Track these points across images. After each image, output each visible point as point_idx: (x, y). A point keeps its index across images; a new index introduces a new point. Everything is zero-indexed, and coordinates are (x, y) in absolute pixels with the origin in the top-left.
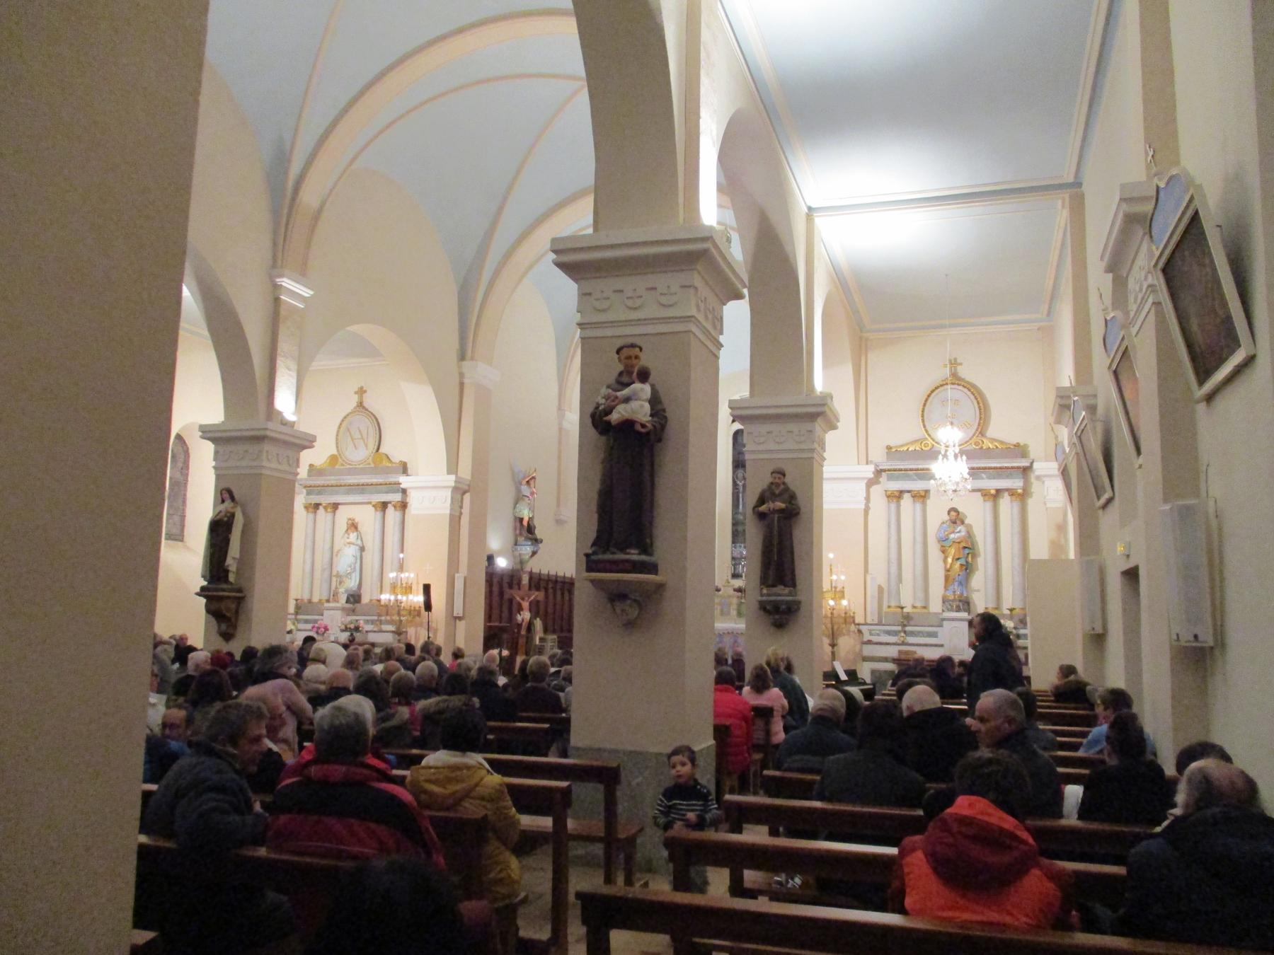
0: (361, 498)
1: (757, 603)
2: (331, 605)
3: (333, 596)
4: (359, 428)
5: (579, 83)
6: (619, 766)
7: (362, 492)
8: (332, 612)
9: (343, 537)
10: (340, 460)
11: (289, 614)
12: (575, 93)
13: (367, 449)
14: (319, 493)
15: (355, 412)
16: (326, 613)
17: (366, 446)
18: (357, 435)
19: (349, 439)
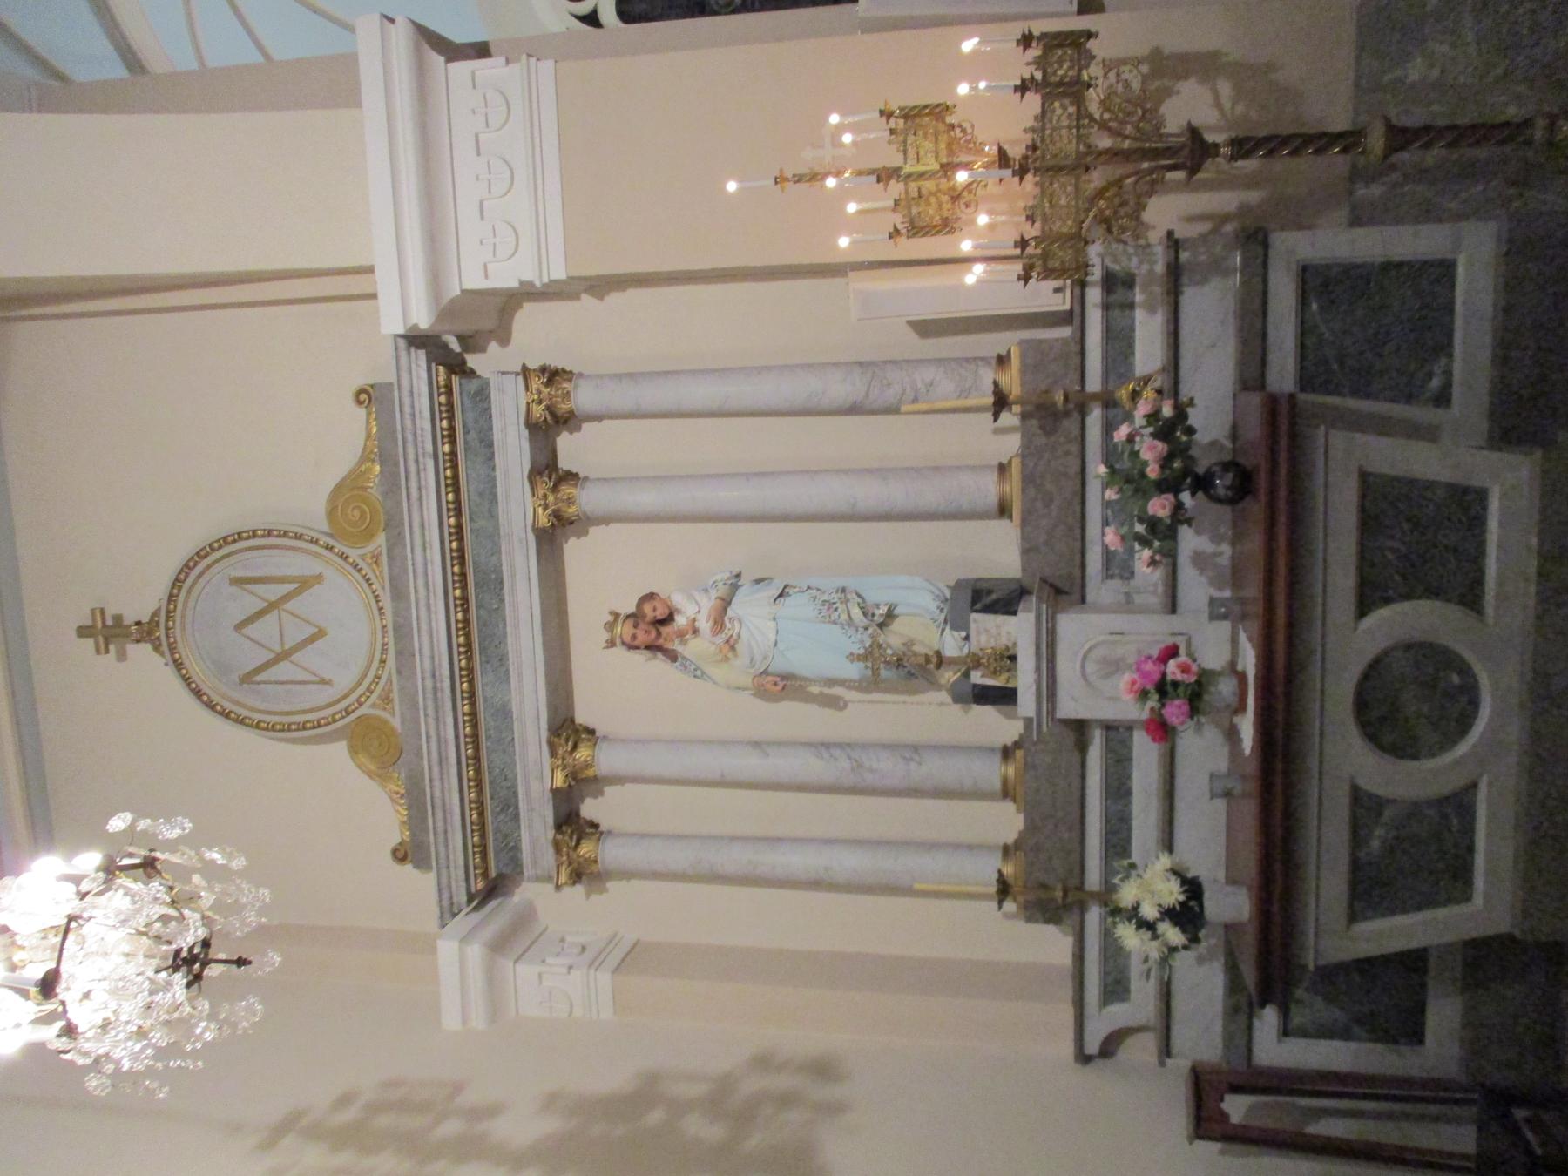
0: (521, 586)
1: (1101, 131)
2: (1025, 679)
3: (848, 297)
4: (239, 627)
5: (284, 614)
6: (1191, 1143)
7: (493, 583)
8: (1067, 669)
9: (699, 674)
10: (364, 710)
11: (907, 192)
12: (287, 611)
13: (318, 578)
14: (509, 806)
15: (172, 649)
16: (1068, 708)
17: (305, 583)
18: (266, 629)
19: (283, 670)
